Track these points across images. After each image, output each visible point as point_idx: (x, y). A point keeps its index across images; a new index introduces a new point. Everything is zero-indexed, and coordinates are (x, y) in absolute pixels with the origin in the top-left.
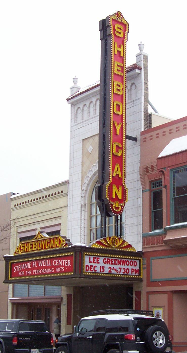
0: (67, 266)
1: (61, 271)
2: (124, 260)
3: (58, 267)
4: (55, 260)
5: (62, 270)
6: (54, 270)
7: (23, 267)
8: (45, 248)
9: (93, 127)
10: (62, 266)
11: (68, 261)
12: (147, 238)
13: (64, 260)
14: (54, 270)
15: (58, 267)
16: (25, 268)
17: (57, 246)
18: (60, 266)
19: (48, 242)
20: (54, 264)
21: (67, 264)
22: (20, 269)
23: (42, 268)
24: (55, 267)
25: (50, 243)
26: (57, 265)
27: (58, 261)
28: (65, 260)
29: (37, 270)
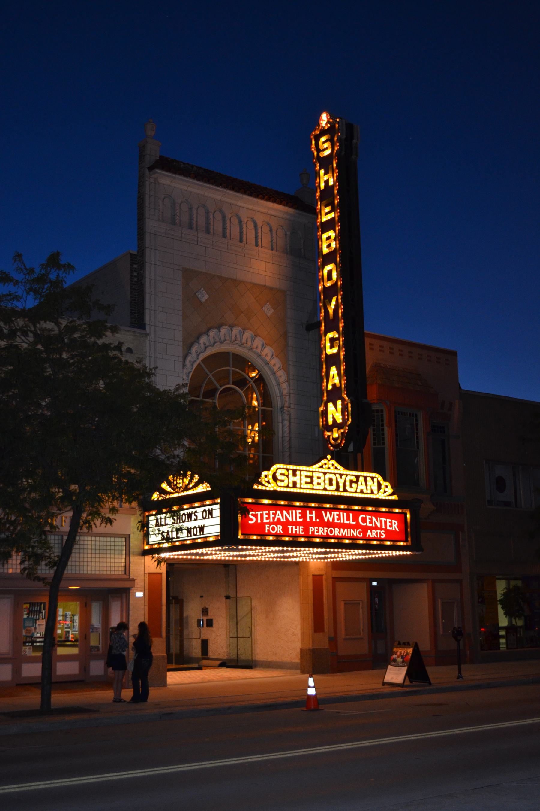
0: (340, 523)
1: (379, 536)
2: (300, 515)
3: (371, 528)
4: (364, 516)
5: (381, 535)
6: (362, 534)
7: (277, 517)
8: (345, 490)
9: (185, 632)
10: (381, 529)
11: (269, 512)
12: (159, 517)
13: (259, 513)
14: (362, 534)
15: (371, 528)
16: (285, 520)
17: (372, 493)
18: (376, 528)
19: (352, 482)
20: (363, 523)
21: (391, 526)
22: (268, 518)
23: (329, 525)
24: (365, 529)
25: (357, 482)
26: (368, 525)
27: (371, 519)
28: (262, 512)
29: (320, 528)
